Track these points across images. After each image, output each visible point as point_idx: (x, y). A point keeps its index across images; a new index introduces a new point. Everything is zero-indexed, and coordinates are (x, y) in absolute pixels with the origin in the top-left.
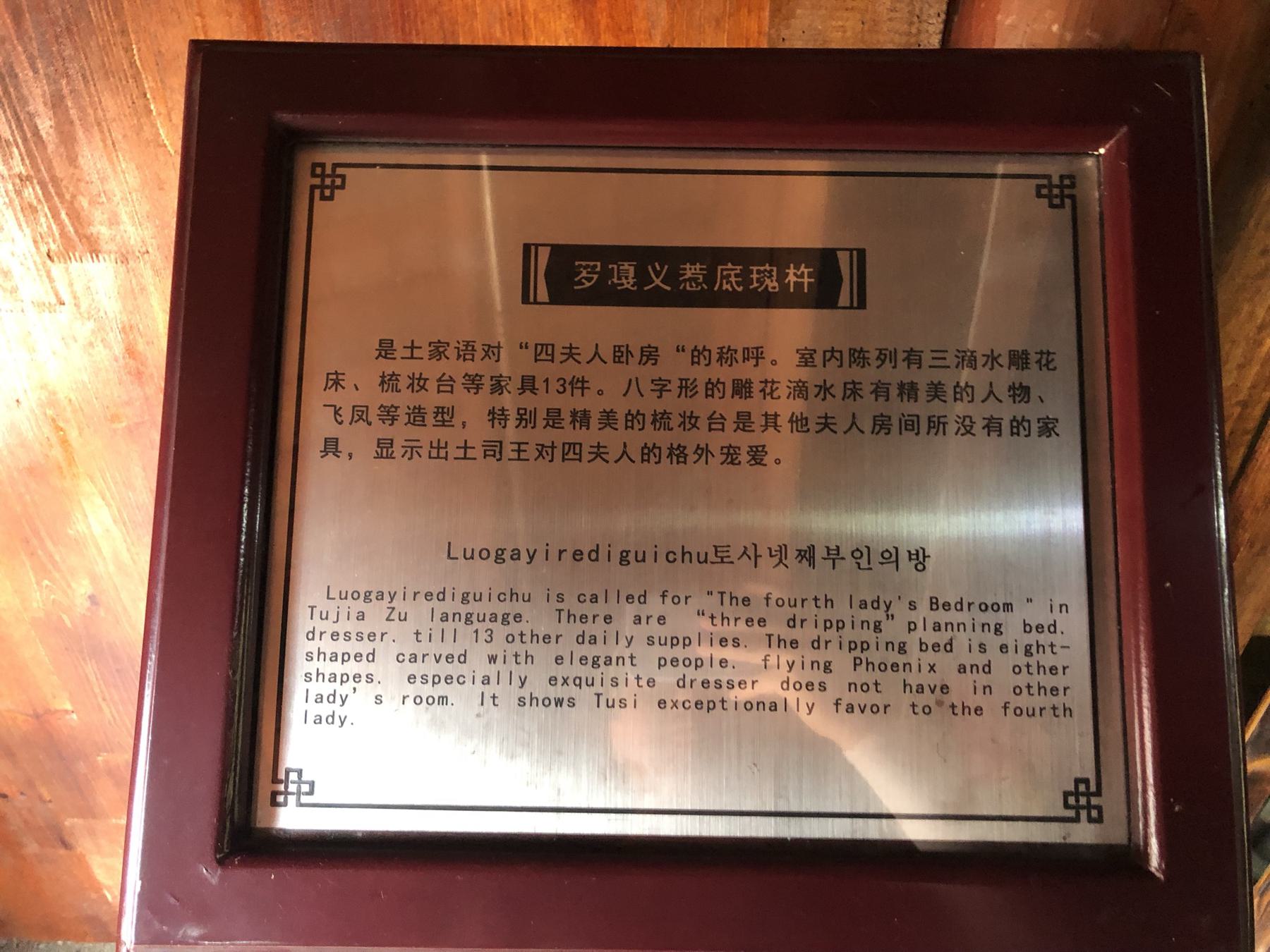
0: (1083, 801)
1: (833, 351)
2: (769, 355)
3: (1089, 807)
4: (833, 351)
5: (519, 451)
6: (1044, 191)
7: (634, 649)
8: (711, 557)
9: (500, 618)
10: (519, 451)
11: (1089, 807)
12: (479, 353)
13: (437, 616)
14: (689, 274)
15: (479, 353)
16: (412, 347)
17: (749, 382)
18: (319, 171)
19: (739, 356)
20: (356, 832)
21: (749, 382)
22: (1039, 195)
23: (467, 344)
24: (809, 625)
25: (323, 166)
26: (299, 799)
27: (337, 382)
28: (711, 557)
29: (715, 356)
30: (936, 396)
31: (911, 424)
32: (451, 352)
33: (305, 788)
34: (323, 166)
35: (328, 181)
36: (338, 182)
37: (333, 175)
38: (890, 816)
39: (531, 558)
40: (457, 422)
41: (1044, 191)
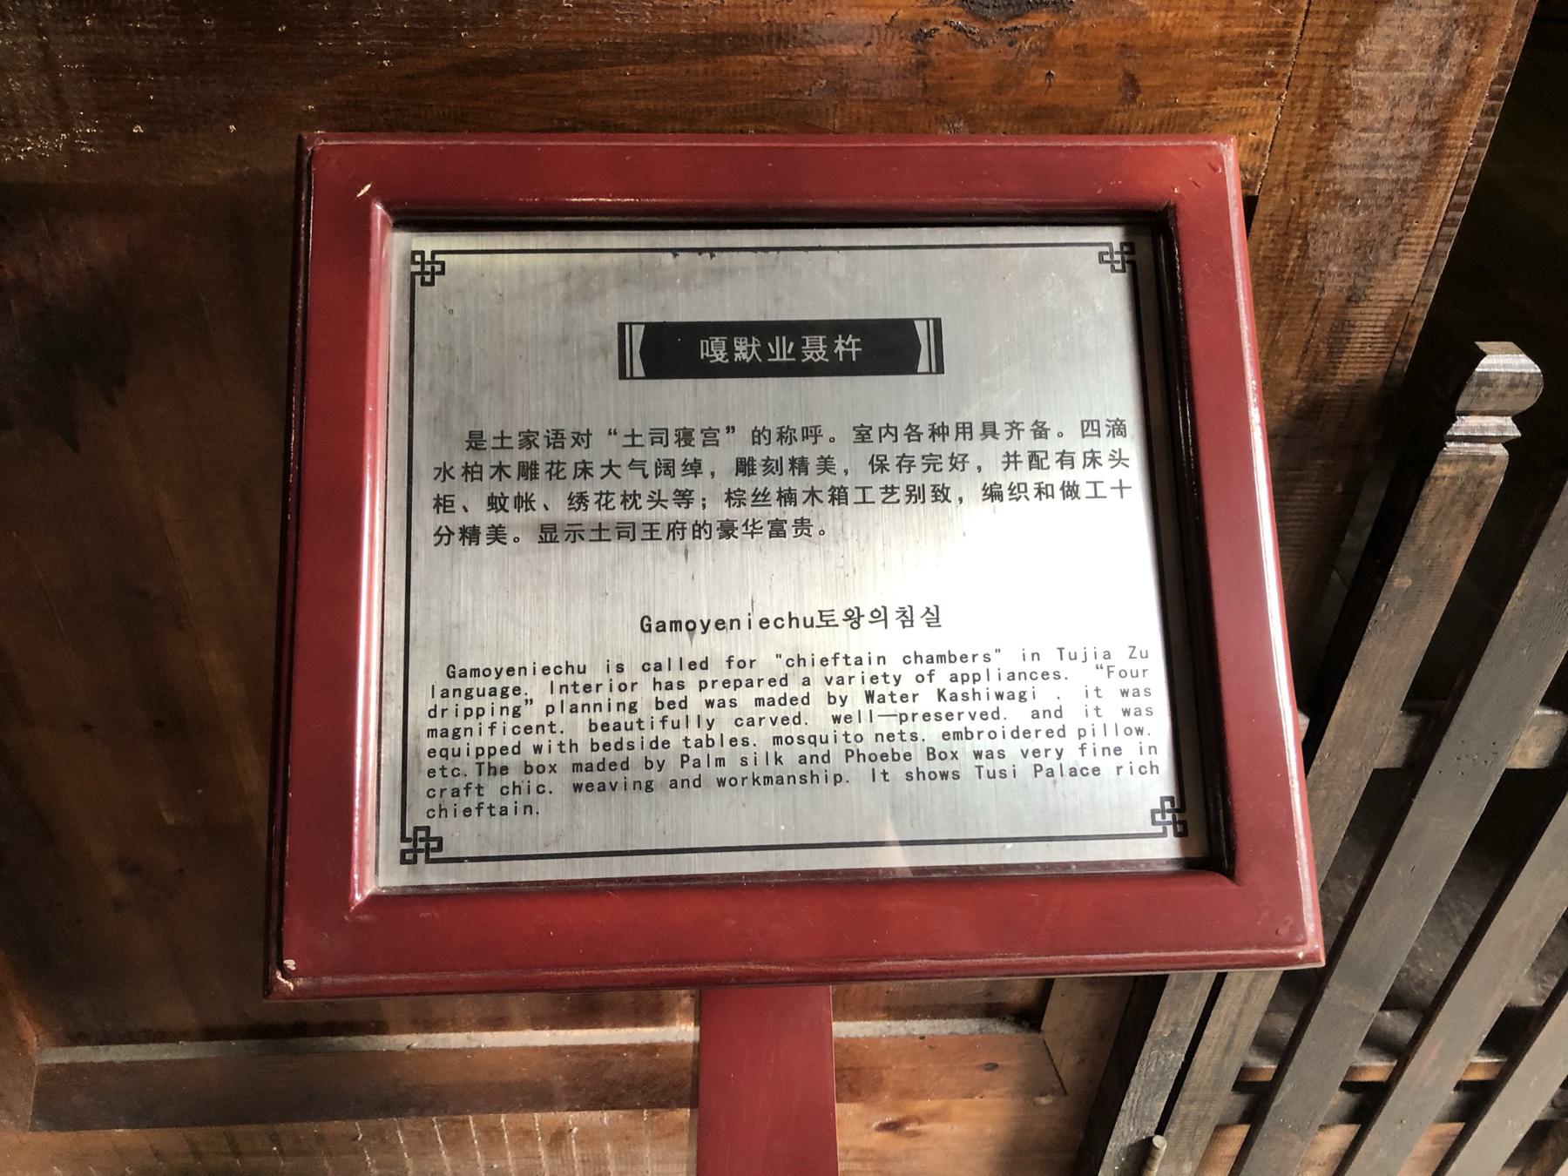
0: (421, 845)
1: (888, 427)
2: (827, 433)
3: (415, 851)
4: (888, 427)
5: (652, 531)
6: (1107, 258)
7: (658, 715)
8: (817, 622)
9: (499, 693)
10: (652, 531)
11: (415, 851)
12: (569, 441)
13: (557, 688)
14: (745, 356)
15: (569, 441)
16: (502, 438)
17: (535, 464)
18: (418, 258)
19: (798, 435)
20: (893, 870)
21: (752, 459)
22: (1101, 261)
23: (557, 432)
24: (605, 689)
25: (422, 253)
26: (427, 855)
27: (1094, 460)
28: (817, 622)
29: (774, 436)
30: (826, 469)
31: (915, 494)
32: (540, 441)
33: (434, 844)
34: (422, 253)
35: (428, 268)
36: (438, 268)
37: (433, 262)
38: (903, 843)
39: (706, 629)
40: (458, 507)
41: (1107, 258)
